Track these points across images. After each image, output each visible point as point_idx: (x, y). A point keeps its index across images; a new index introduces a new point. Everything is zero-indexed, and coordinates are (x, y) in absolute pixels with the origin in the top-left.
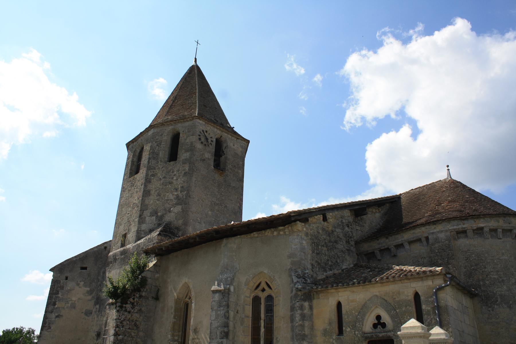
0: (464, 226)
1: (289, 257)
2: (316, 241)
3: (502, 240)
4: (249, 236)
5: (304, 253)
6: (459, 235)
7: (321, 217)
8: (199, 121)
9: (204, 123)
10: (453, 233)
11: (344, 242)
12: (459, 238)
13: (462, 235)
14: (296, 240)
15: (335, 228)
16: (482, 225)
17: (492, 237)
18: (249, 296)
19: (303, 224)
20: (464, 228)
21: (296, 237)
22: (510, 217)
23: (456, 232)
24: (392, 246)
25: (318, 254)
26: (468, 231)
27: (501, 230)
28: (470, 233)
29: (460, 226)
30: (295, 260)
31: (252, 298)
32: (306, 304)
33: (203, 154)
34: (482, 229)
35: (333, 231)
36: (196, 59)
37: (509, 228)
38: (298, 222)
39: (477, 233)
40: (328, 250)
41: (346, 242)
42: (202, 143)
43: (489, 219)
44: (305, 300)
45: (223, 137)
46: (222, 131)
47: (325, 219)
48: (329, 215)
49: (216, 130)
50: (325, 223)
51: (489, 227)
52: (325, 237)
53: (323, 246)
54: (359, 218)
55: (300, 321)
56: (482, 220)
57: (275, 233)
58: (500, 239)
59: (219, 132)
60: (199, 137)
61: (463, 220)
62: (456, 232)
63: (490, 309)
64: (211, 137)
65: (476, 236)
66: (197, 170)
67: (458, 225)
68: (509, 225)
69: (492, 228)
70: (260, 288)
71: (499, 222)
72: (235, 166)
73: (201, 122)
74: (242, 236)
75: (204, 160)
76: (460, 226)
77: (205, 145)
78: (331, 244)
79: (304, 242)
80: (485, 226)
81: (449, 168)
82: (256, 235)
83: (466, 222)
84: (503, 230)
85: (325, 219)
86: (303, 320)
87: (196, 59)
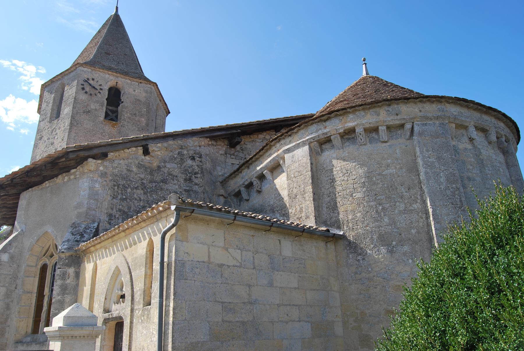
0: (325, 131)
1: (76, 208)
2: (122, 182)
3: (388, 144)
4: (40, 187)
5: (97, 200)
6: (323, 146)
7: (140, 150)
8: (83, 69)
9: (90, 70)
10: (312, 145)
11: (182, 181)
12: (322, 151)
13: (327, 146)
14: (86, 184)
15: (165, 162)
16: (350, 125)
17: (371, 142)
18: (32, 264)
19: (100, 162)
20: (326, 133)
21: (85, 179)
22: (397, 104)
23: (318, 141)
24: (254, 179)
25: (122, 200)
26: (332, 137)
27: (384, 128)
28: (337, 141)
29: (320, 132)
30: (81, 211)
31: (39, 267)
32: (71, 271)
33: (88, 105)
34: (352, 131)
35: (159, 167)
36: (117, 8)
37: (398, 122)
38: (90, 160)
39: (348, 139)
40: (145, 193)
41: (185, 180)
42: (86, 92)
43: (362, 113)
44: (69, 265)
45: (119, 83)
46: (117, 77)
47: (146, 152)
48: (152, 147)
49: (107, 76)
50: (147, 158)
51: (363, 124)
52: (142, 176)
53: (137, 188)
54: (238, 147)
55: (58, 295)
56: (351, 116)
57: (66, 178)
58: (386, 142)
59: (112, 78)
60: (82, 87)
61: (325, 121)
62: (318, 141)
63: (359, 258)
64: (101, 85)
65: (347, 144)
66: (78, 124)
67: (317, 131)
68: (396, 117)
69: (367, 126)
70: (49, 253)
71: (378, 115)
72: (135, 114)
73: (86, 69)
74: (34, 188)
75: (89, 112)
76: (320, 132)
77: (91, 95)
78: (154, 184)
79: (97, 186)
80: (357, 125)
81: (366, 62)
82: (47, 185)
83: (328, 123)
84: (389, 128)
85: (146, 152)
86: (63, 294)
87: (117, 8)
